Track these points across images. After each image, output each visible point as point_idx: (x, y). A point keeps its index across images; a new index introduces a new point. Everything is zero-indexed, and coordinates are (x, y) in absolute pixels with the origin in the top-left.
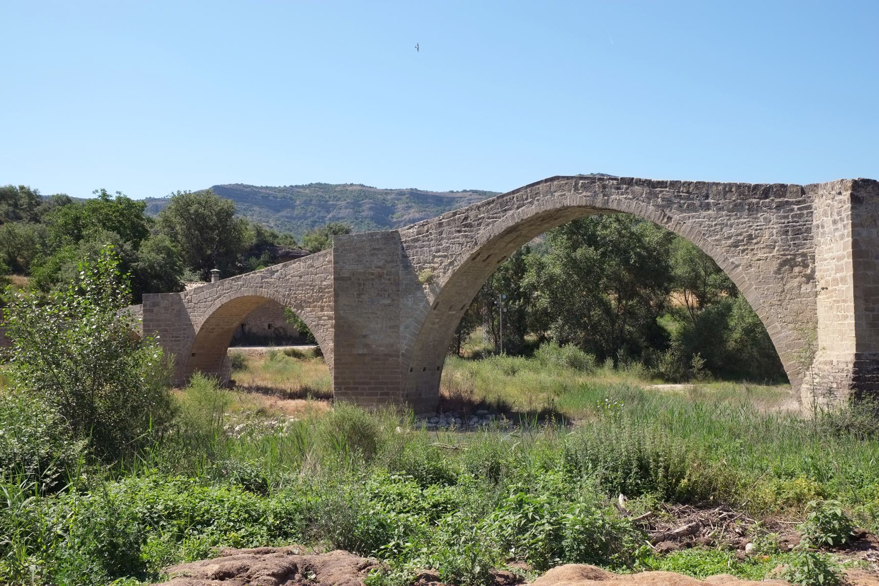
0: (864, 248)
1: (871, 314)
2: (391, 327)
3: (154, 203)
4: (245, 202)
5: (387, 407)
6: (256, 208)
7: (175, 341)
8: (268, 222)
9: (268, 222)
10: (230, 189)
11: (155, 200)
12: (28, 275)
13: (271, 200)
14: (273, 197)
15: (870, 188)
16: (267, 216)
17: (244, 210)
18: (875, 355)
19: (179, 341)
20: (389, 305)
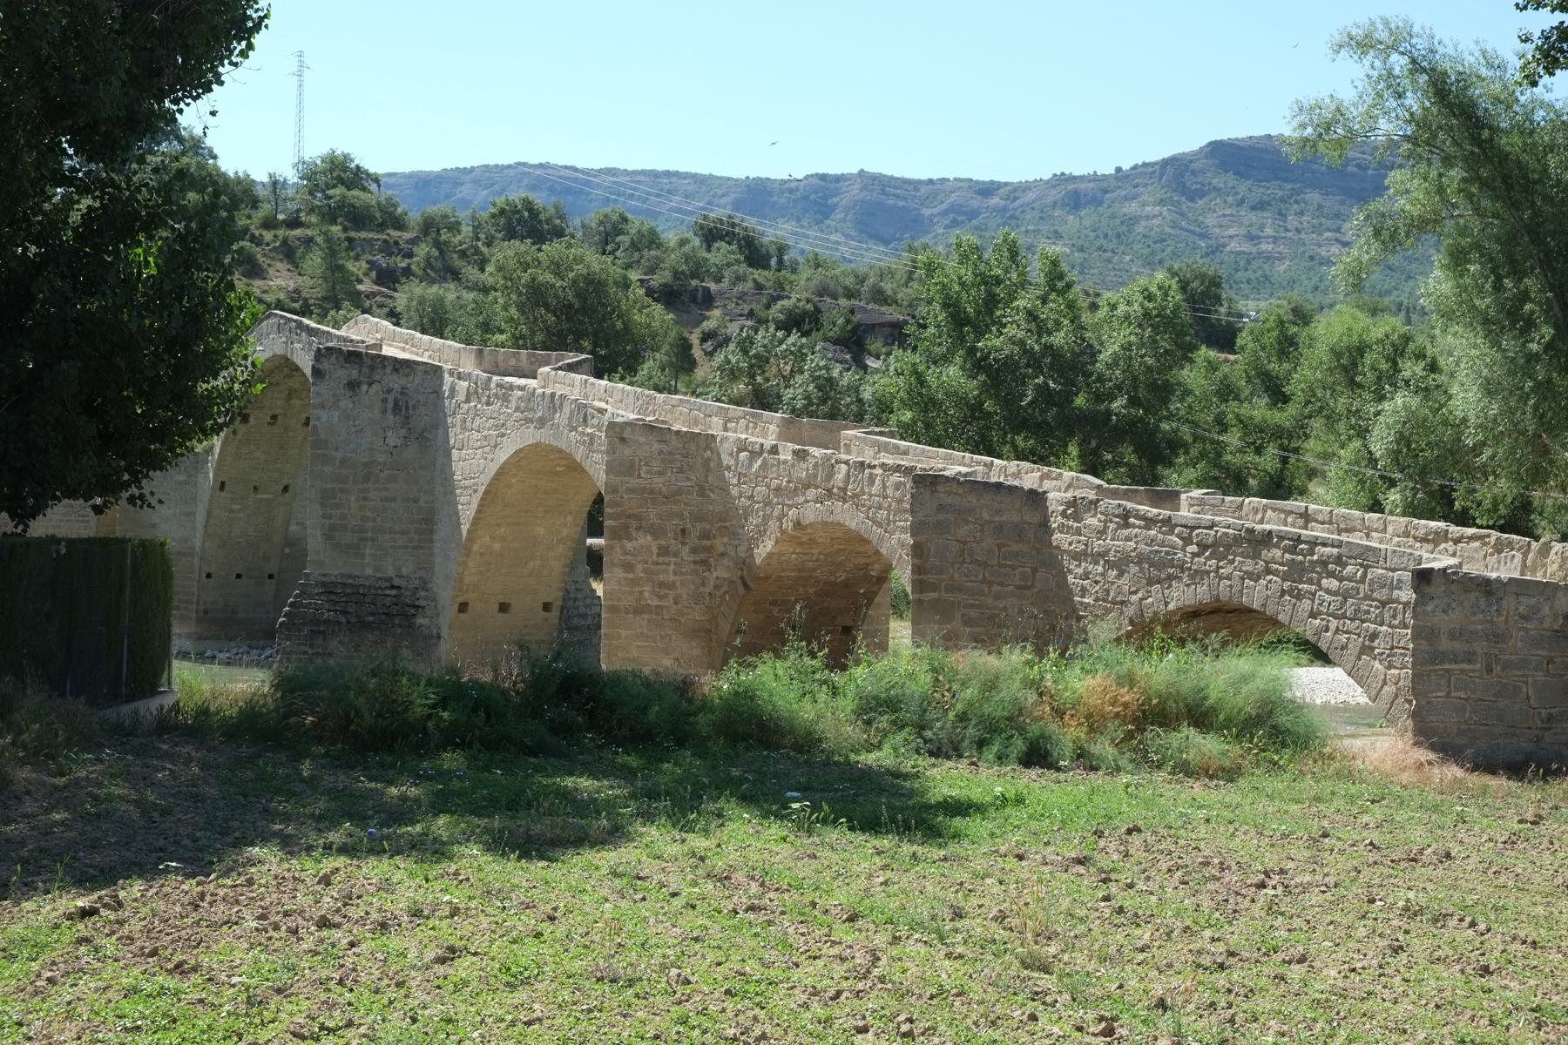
0: (323, 436)
1: (328, 522)
2: (187, 514)
3: (1071, 187)
4: (1285, 180)
5: (1303, 697)
6: (1313, 197)
7: (83, 522)
8: (1338, 230)
9: (1338, 230)
10: (1251, 148)
11: (1073, 178)
12: (535, 378)
13: (1353, 175)
14: (1358, 166)
15: (333, 358)
16: (1337, 216)
17: (1282, 200)
18: (325, 575)
19: (88, 522)
20: (185, 483)
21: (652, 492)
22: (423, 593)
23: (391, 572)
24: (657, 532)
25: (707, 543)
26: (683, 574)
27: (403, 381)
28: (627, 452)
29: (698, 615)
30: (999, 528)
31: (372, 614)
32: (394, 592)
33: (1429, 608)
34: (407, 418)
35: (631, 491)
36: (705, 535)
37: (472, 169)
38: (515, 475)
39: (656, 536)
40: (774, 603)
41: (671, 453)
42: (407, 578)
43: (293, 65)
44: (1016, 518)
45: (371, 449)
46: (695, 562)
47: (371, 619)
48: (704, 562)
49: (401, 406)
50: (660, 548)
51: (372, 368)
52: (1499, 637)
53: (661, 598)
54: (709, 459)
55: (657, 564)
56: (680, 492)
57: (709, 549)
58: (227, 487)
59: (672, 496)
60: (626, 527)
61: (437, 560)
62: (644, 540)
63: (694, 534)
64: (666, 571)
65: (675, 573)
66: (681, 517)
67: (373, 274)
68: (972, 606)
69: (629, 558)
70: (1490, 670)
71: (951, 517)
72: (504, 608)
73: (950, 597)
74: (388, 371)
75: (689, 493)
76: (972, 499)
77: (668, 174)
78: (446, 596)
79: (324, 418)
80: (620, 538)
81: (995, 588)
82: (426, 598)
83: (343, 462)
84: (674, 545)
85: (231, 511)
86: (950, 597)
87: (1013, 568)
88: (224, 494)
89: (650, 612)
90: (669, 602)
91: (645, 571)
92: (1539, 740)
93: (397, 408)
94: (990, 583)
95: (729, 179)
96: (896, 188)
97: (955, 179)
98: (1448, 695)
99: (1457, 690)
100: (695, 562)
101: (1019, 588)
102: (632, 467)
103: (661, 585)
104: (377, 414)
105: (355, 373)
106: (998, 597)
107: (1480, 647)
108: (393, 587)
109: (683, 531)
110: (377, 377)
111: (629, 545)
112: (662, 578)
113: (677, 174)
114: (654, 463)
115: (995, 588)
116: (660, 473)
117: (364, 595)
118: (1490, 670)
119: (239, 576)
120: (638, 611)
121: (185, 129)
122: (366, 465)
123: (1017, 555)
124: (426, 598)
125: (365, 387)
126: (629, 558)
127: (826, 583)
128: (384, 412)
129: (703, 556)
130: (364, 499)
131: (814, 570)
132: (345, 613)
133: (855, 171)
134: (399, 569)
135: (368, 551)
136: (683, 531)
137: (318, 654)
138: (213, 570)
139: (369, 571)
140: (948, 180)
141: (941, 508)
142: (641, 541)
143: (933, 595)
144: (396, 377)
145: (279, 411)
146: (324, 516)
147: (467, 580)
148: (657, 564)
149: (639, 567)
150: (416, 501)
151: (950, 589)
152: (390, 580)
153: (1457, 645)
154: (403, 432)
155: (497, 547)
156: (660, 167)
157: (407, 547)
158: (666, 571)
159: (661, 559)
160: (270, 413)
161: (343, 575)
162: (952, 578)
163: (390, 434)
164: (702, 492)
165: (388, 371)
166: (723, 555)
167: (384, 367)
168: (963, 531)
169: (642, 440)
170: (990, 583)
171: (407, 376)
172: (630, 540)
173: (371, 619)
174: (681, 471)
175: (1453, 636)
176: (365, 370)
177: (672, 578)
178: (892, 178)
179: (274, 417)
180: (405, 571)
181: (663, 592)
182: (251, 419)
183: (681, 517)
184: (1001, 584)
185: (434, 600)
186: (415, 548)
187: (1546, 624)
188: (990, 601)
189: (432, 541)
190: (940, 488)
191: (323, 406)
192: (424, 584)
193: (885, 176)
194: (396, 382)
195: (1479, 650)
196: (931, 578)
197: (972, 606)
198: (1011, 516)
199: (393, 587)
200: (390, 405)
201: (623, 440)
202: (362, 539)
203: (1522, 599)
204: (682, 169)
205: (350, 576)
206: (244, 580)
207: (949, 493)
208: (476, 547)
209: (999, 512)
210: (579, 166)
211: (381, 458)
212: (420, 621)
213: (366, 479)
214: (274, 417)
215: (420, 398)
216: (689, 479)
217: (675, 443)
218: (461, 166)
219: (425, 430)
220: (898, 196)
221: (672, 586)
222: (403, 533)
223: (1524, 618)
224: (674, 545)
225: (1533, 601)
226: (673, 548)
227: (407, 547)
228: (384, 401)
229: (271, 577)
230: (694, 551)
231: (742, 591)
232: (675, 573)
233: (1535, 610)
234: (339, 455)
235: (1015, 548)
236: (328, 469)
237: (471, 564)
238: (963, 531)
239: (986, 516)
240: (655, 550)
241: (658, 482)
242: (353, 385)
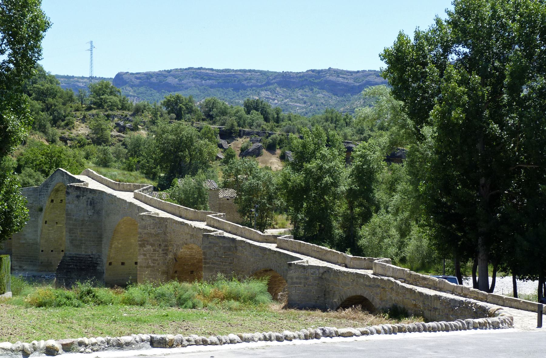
0: (69, 212)
15: (72, 188)
21: (151, 234)
22: (99, 260)
23: (90, 253)
24: (152, 245)
25: (167, 248)
26: (160, 257)
27: (93, 195)
28: (144, 223)
29: (164, 268)
30: (224, 248)
31: (84, 266)
32: (91, 259)
33: (291, 272)
34: (94, 207)
35: (145, 234)
36: (166, 246)
37: (171, 71)
38: (123, 225)
39: (152, 246)
40: (184, 265)
41: (156, 223)
42: (94, 255)
43: (89, 47)
44: (229, 245)
45: (84, 216)
46: (163, 253)
47: (84, 267)
48: (165, 253)
49: (92, 203)
50: (153, 249)
51: (84, 192)
52: (307, 279)
53: (154, 263)
54: (167, 224)
55: (153, 254)
56: (159, 234)
57: (167, 250)
58: (47, 223)
59: (157, 235)
60: (144, 244)
61: (103, 250)
62: (149, 247)
63: (163, 245)
64: (155, 256)
65: (158, 257)
66: (159, 241)
67: (118, 128)
68: (218, 268)
69: (145, 252)
70: (305, 286)
71: (212, 245)
72: (123, 264)
73: (212, 266)
74: (88, 192)
75: (162, 234)
76: (218, 240)
77: (250, 71)
78: (105, 260)
79: (70, 206)
80: (142, 247)
81: (224, 263)
82: (100, 261)
83: (75, 220)
84: (157, 249)
85: (49, 230)
86: (212, 266)
87: (228, 258)
88: (46, 225)
89: (151, 267)
90: (156, 265)
91: (150, 256)
92: (316, 302)
93: (91, 204)
94: (223, 262)
95: (275, 72)
96: (343, 74)
97: (369, 71)
98: (296, 292)
99: (298, 291)
100: (163, 253)
101: (230, 263)
102: (145, 227)
103: (154, 260)
104: (85, 205)
105: (79, 193)
106: (224, 265)
107: (303, 281)
108: (90, 258)
109: (160, 245)
110: (85, 194)
111: (145, 249)
112: (154, 258)
113: (254, 71)
114: (151, 226)
115: (224, 263)
116: (153, 229)
117: (82, 260)
118: (305, 286)
119: (52, 251)
120: (148, 267)
121: (47, 73)
122: (82, 221)
123: (229, 255)
124: (100, 261)
125: (81, 197)
126: (145, 252)
127: (199, 259)
128: (87, 205)
129: (165, 252)
130: (82, 231)
131: (195, 255)
132: (76, 265)
133: (327, 68)
134: (92, 252)
135: (83, 247)
136: (160, 245)
137: (68, 278)
138: (43, 249)
139: (83, 253)
140: (366, 71)
141: (210, 243)
142: (148, 248)
143: (208, 265)
144: (90, 194)
145: (63, 198)
146: (70, 236)
147: (111, 256)
148: (153, 254)
149: (148, 255)
150: (97, 231)
151: (212, 264)
152: (89, 255)
153: (298, 281)
154: (93, 211)
155: (120, 246)
156: (247, 69)
157: (94, 246)
158: (155, 256)
159: (154, 253)
160: (60, 199)
161: (75, 254)
162: (213, 261)
163: (89, 211)
164: (165, 234)
165: (88, 192)
166: (171, 251)
167: (87, 191)
168: (215, 249)
169: (148, 219)
170: (223, 262)
171: (94, 194)
172: (145, 247)
173: (84, 267)
174: (159, 228)
175: (296, 278)
176: (82, 192)
177: (157, 258)
178: (343, 71)
179: (62, 200)
180: (94, 253)
181: (154, 262)
182: (54, 201)
183: (159, 241)
184: (225, 262)
185: (102, 261)
186: (97, 246)
187: (317, 275)
188: (222, 267)
189: (101, 244)
190: (210, 238)
191: (69, 203)
192: (99, 257)
193: (340, 70)
194: (91, 196)
195: (302, 282)
196: (208, 261)
197: (218, 268)
198: (227, 245)
199: (90, 258)
200: (89, 203)
201: (143, 219)
202: (82, 243)
203: (312, 270)
204: (256, 69)
205: (78, 254)
206: (54, 252)
207: (212, 239)
208: (113, 246)
209: (224, 244)
210: (214, 68)
211: (86, 219)
212: (98, 268)
213: (82, 225)
214: (62, 200)
215: (98, 201)
216: (161, 230)
217: (157, 220)
218: (167, 70)
219: (99, 210)
220: (344, 78)
221: (157, 260)
222: (93, 241)
223: (312, 274)
224: (157, 249)
225: (314, 270)
226: (157, 250)
227: (94, 246)
228: (87, 201)
229: (62, 251)
230: (163, 250)
231: (175, 261)
232: (158, 257)
233: (315, 272)
234: (74, 218)
235: (229, 253)
236: (71, 222)
237: (112, 251)
238: (215, 249)
239: (221, 244)
240: (152, 250)
241: (153, 231)
242: (78, 197)
